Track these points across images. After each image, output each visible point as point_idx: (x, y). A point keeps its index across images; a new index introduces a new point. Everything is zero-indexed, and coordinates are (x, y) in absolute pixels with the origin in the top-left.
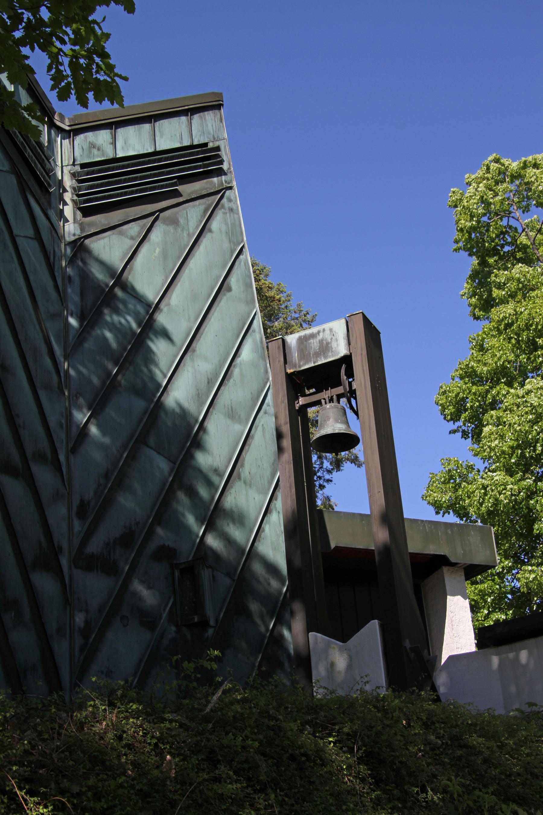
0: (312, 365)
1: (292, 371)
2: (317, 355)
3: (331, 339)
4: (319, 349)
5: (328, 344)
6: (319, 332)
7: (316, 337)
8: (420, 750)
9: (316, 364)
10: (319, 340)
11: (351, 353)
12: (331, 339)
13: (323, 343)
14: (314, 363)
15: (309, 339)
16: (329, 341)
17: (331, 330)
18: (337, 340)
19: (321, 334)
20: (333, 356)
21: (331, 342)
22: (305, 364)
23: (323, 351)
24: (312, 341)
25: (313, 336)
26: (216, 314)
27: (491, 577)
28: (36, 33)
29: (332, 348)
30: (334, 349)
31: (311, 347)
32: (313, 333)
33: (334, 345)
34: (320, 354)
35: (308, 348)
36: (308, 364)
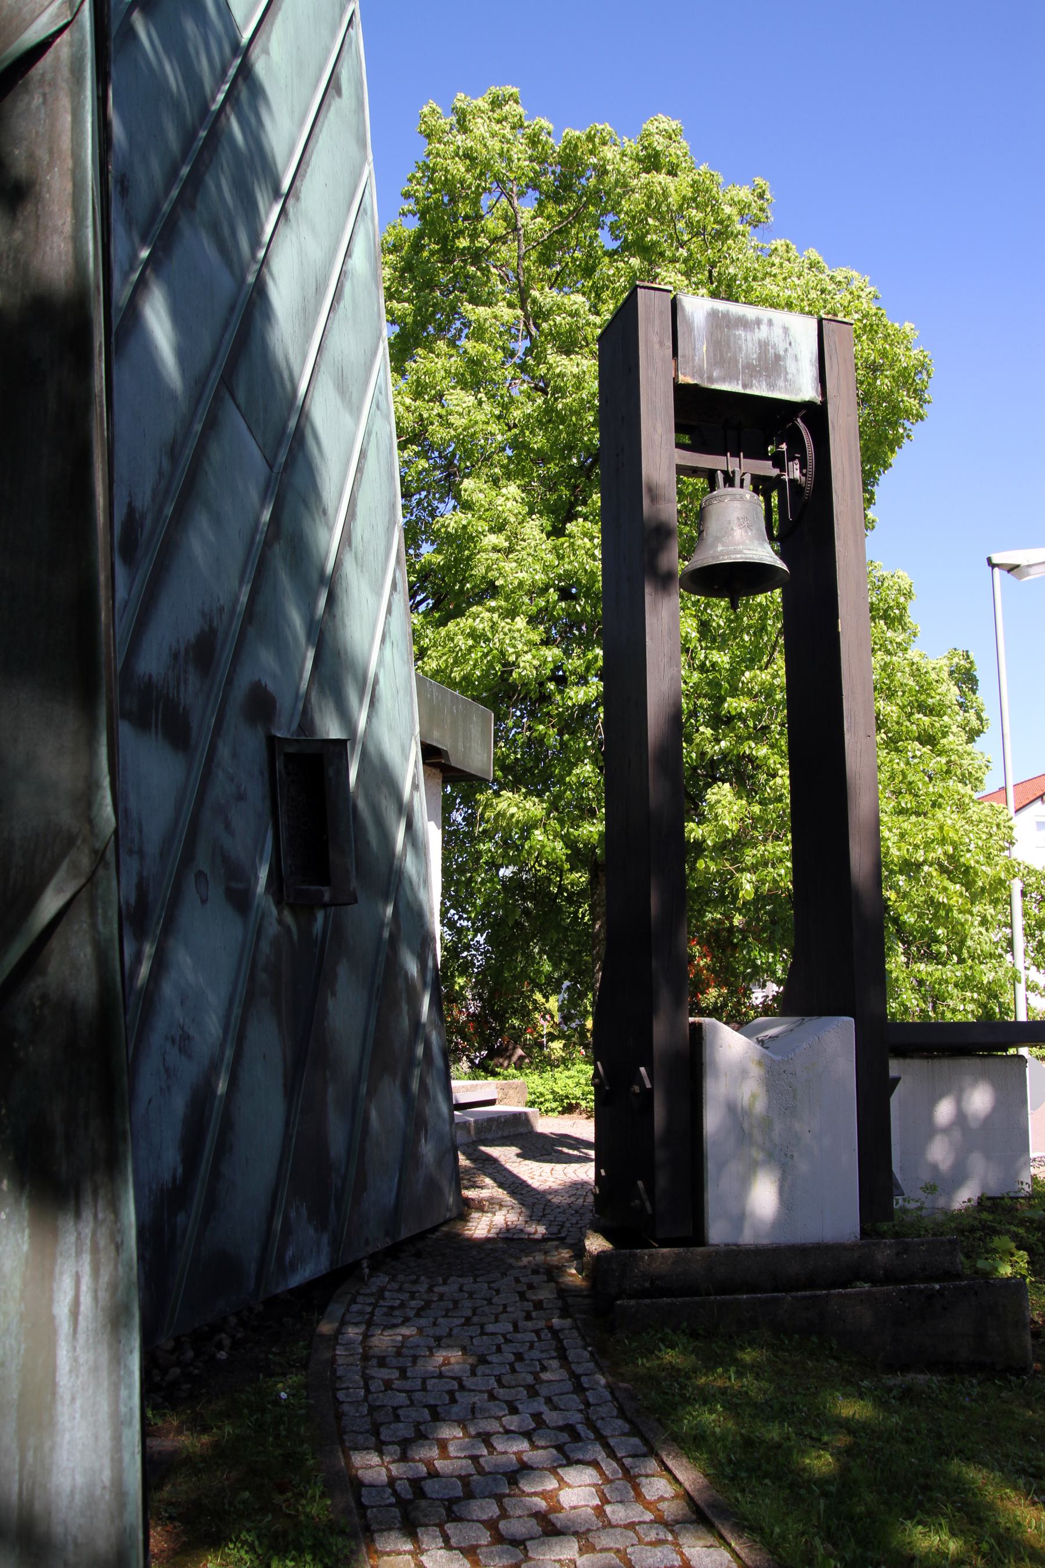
0: (739, 389)
1: (690, 381)
2: (753, 371)
3: (786, 350)
4: (759, 359)
5: (778, 358)
6: (758, 322)
7: (752, 330)
9: (748, 392)
10: (759, 341)
11: (825, 403)
12: (786, 350)
13: (766, 352)
14: (745, 386)
16: (782, 353)
17: (786, 330)
19: (764, 327)
20: (786, 391)
21: (784, 359)
22: (723, 380)
23: (767, 370)
24: (740, 332)
25: (743, 323)
29: (787, 373)
30: (789, 377)
31: (740, 348)
32: (744, 316)
33: (790, 365)
35: (732, 345)
36: (730, 382)
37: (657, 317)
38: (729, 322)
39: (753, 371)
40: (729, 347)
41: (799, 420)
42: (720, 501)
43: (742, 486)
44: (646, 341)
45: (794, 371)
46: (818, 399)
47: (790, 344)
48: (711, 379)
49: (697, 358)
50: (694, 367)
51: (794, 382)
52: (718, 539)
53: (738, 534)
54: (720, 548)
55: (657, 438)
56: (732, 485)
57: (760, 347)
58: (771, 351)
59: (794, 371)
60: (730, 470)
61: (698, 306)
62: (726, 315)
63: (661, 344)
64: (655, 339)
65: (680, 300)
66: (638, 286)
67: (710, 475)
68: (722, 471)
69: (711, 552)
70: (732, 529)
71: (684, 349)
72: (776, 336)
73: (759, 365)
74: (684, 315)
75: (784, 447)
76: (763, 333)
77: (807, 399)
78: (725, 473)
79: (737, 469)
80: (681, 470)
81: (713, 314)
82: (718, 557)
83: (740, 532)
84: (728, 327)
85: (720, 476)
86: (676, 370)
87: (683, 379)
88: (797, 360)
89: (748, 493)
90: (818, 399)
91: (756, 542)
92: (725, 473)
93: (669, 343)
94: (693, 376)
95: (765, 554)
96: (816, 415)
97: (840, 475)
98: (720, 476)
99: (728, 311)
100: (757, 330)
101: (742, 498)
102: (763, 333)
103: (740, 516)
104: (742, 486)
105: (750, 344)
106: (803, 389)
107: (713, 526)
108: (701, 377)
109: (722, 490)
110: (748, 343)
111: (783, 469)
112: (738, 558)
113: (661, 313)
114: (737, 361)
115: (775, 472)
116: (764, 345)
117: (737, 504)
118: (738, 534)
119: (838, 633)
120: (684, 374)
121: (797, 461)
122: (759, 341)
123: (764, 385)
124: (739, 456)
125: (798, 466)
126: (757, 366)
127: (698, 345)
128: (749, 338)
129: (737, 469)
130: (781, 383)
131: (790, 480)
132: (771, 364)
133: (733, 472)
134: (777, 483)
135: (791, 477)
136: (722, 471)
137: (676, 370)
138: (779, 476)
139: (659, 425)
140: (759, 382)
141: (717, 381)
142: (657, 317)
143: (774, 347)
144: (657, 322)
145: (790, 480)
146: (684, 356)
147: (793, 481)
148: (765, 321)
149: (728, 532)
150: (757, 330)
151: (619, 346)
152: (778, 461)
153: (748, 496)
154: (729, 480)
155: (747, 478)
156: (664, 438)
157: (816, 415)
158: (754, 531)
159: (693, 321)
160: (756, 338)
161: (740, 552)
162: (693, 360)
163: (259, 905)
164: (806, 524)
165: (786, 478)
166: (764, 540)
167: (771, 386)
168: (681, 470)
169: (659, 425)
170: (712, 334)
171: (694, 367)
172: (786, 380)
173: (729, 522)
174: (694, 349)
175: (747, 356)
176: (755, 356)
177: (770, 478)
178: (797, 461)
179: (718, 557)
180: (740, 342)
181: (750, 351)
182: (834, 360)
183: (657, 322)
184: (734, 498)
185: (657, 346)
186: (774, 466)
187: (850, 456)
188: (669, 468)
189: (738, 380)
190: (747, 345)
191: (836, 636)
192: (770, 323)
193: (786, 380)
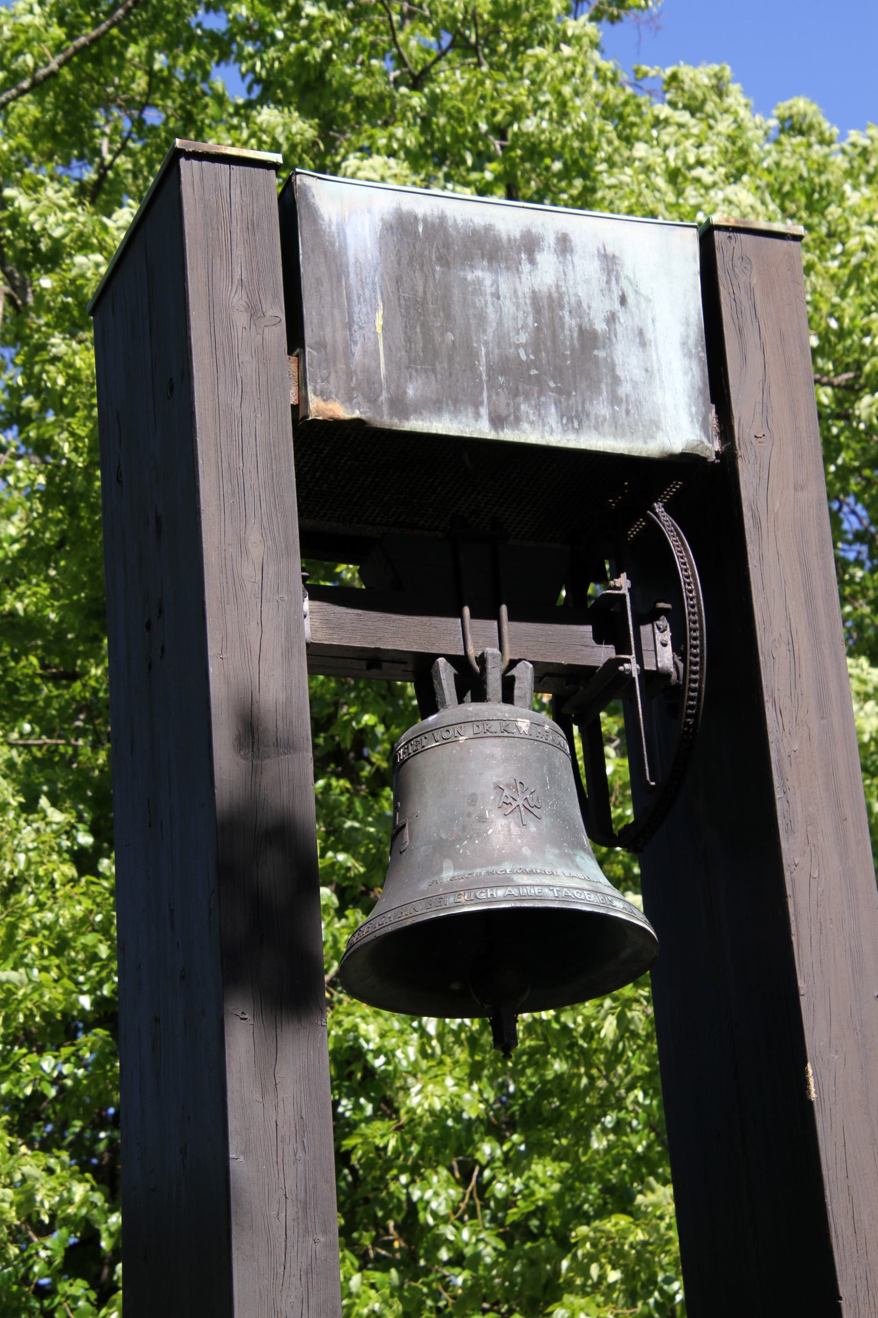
0: (480, 429)
1: (340, 411)
2: (519, 379)
3: (612, 319)
4: (536, 344)
5: (589, 339)
6: (530, 245)
7: (514, 267)
8: (18, 479)
9: (508, 435)
10: (535, 296)
11: (728, 458)
12: (612, 319)
13: (555, 325)
14: (497, 421)
15: (468, 260)
16: (600, 326)
17: (609, 263)
18: (642, 339)
19: (547, 259)
20: (617, 429)
21: (608, 340)
22: (436, 406)
23: (558, 373)
24: (481, 274)
25: (486, 247)
26: (304, 226)
27: (589, 1107)
28: (111, 1104)
29: (616, 381)
30: (624, 390)
31: (482, 318)
32: (488, 228)
33: (626, 358)
34: (538, 381)
35: (457, 309)
36: (456, 413)
37: (238, 236)
38: (447, 245)
39: (519, 379)
40: (448, 317)
41: (659, 507)
42: (446, 741)
43: (508, 697)
44: (211, 305)
45: (638, 374)
46: (712, 448)
47: (623, 300)
48: (399, 405)
49: (357, 350)
50: (350, 374)
51: (639, 404)
52: (443, 849)
53: (501, 829)
54: (448, 874)
55: (249, 572)
56: (480, 696)
57: (538, 311)
58: (570, 321)
59: (638, 374)
60: (473, 653)
61: (359, 205)
62: (438, 228)
63: (254, 312)
64: (238, 300)
65: (305, 190)
66: (179, 153)
67: (422, 666)
68: (451, 659)
69: (424, 886)
70: (482, 819)
71: (321, 325)
72: (583, 279)
73: (536, 364)
74: (318, 232)
75: (623, 583)
76: (545, 273)
77: (677, 447)
78: (459, 662)
79: (492, 651)
80: (321, 658)
81: (401, 229)
82: (440, 898)
83: (506, 819)
84: (444, 261)
85: (446, 673)
86: (302, 384)
87: (326, 407)
88: (643, 344)
89: (527, 718)
90: (712, 448)
91: (551, 853)
92: (459, 662)
93: (277, 311)
94: (349, 400)
95: (579, 881)
96: (705, 489)
97: (782, 652)
98: (446, 673)
99: (443, 218)
100: (526, 267)
101: (506, 732)
102: (545, 273)
103: (503, 781)
104: (508, 697)
105: (508, 306)
106: (670, 421)
107: (429, 814)
108: (372, 400)
109: (453, 710)
110: (503, 301)
111: (622, 647)
112: (500, 898)
113: (251, 227)
114: (473, 355)
115: (604, 653)
116: (547, 307)
117: (493, 748)
118: (501, 829)
119: (807, 1108)
120: (325, 396)
121: (663, 622)
122: (535, 296)
123: (552, 416)
124: (497, 617)
125: (667, 636)
126: (529, 365)
127: (360, 311)
128: (504, 289)
129: (492, 651)
130: (601, 408)
131: (644, 674)
132: (573, 356)
133: (482, 660)
134: (607, 685)
135: (649, 666)
136: (451, 659)
137: (302, 384)
138: (612, 664)
139: (254, 536)
140: (538, 407)
141: (418, 409)
142: (238, 236)
143: (578, 310)
144: (239, 252)
145: (644, 674)
146: (321, 345)
147: (654, 679)
148: (550, 240)
149: (470, 825)
150: (526, 267)
151: (143, 307)
152: (609, 625)
153: (524, 725)
154: (471, 683)
155: (524, 675)
156: (270, 570)
157: (705, 489)
158: (546, 821)
159: (344, 247)
160: (524, 289)
161: (505, 882)
162: (348, 354)
163: (357, 260)
164: (696, 790)
165: (633, 668)
166: (577, 845)
167: (574, 418)
168: (321, 658)
169: (254, 536)
170: (398, 281)
171: (350, 374)
172: (615, 400)
173: (473, 800)
174: (349, 325)
175: (501, 338)
176: (523, 338)
177: (589, 671)
178: (663, 622)
179: (440, 898)
180: (479, 302)
181: (508, 324)
182: (750, 331)
183: (239, 252)
184: (484, 730)
185: (241, 319)
186: (599, 638)
187: (810, 598)
188: (287, 654)
189: (477, 405)
190: (499, 310)
191: (804, 1112)
192: (564, 245)
193: (615, 400)
